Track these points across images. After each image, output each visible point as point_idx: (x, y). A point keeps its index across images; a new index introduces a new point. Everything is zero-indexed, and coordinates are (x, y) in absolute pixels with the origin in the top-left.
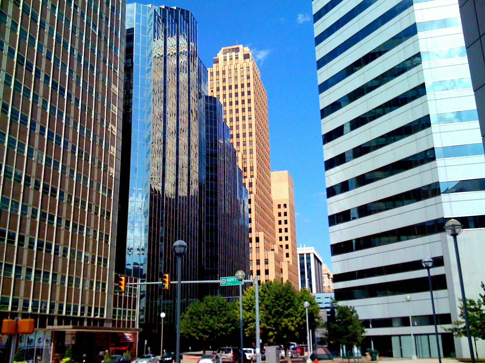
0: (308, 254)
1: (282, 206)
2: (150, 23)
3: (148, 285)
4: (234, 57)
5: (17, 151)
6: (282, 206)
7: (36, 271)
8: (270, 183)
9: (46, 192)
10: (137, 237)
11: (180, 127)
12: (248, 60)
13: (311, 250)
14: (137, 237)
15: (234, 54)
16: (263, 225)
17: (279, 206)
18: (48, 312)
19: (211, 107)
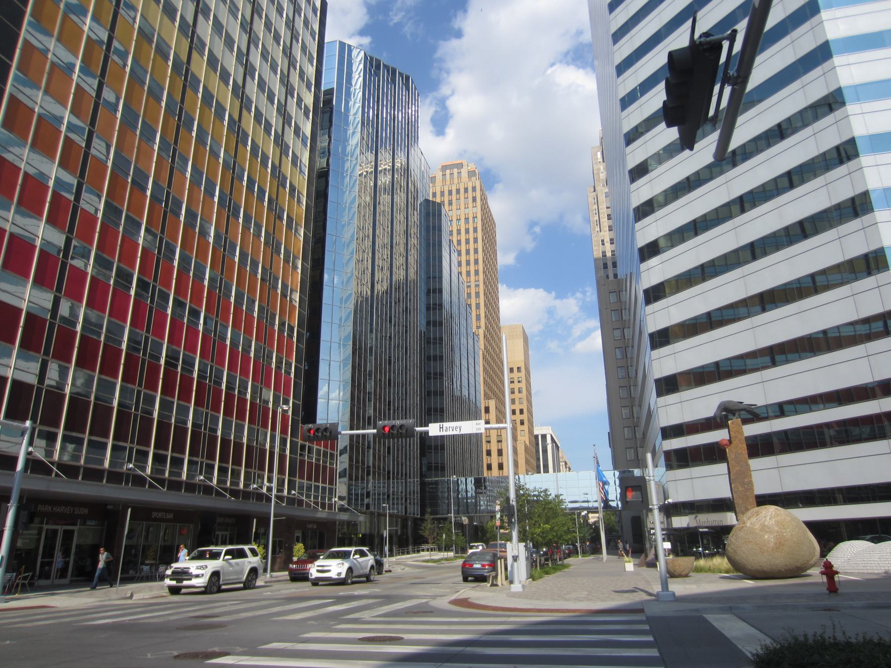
0: (544, 437)
1: (515, 370)
2: (351, 250)
3: (351, 436)
4: (456, 175)
5: (114, 284)
6: (515, 370)
7: (156, 457)
8: (498, 299)
9: (173, 364)
10: (333, 401)
11: (394, 242)
12: (473, 179)
13: (547, 431)
14: (333, 401)
15: (455, 171)
16: (494, 394)
17: (511, 370)
18: (184, 477)
19: (435, 323)
